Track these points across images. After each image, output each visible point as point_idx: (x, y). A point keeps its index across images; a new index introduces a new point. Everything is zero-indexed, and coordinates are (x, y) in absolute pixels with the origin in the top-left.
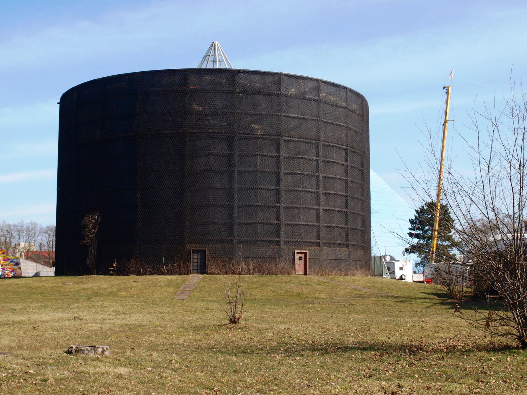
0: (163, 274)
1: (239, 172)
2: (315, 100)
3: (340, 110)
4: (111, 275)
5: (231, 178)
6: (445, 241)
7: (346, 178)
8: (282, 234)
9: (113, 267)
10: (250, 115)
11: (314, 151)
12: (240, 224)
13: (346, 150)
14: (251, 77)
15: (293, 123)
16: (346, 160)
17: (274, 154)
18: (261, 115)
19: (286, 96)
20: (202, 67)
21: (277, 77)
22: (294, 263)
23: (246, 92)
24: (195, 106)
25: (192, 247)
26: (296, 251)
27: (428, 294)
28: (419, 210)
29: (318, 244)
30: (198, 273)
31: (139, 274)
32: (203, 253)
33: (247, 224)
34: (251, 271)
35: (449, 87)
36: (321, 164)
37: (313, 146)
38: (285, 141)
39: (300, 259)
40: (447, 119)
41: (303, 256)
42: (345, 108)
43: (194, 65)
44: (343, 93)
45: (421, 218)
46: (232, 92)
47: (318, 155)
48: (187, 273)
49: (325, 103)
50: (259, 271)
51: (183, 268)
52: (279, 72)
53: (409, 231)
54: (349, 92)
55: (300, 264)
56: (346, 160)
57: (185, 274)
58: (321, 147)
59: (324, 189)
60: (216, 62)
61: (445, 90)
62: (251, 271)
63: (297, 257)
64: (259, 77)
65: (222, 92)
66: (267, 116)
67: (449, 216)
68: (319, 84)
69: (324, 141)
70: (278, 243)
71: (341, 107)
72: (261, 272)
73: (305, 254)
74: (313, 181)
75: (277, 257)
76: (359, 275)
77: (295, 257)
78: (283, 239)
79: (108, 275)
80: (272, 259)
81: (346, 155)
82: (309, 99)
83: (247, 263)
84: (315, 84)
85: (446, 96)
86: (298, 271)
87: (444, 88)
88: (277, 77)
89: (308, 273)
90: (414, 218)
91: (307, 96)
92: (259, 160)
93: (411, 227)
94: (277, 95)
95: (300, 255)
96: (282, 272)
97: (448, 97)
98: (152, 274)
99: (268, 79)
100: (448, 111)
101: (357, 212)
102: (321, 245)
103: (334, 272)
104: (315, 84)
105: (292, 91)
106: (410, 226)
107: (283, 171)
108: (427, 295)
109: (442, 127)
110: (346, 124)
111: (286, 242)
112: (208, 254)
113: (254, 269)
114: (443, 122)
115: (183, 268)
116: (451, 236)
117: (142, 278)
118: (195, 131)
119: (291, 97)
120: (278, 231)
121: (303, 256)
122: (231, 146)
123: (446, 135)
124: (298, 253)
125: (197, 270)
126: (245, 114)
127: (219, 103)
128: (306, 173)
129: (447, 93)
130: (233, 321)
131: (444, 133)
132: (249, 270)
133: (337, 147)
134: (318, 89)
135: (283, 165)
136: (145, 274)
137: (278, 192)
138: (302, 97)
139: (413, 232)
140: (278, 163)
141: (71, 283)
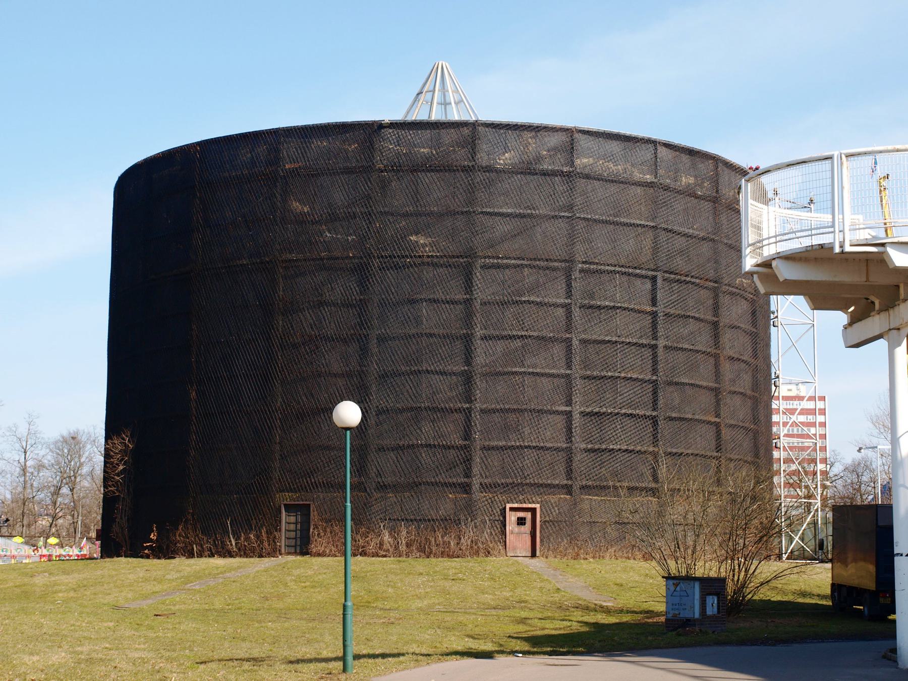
0: (230, 554)
1: (381, 340)
2: (561, 174)
4: (148, 557)
5: (364, 351)
8: (476, 470)
9: (151, 541)
10: (406, 215)
11: (561, 286)
12: (381, 449)
14: (410, 135)
15: (503, 227)
16: (654, 302)
17: (460, 297)
18: (430, 214)
19: (489, 169)
21: (466, 131)
22: (504, 533)
23: (396, 168)
24: (296, 206)
25: (287, 498)
26: (508, 506)
29: (568, 490)
30: (295, 553)
31: (191, 555)
32: (303, 510)
33: (398, 448)
34: (403, 548)
36: (576, 312)
37: (559, 274)
38: (484, 267)
39: (521, 522)
41: (528, 515)
42: (650, 185)
43: (397, 115)
46: (367, 169)
47: (569, 294)
48: (274, 552)
49: (587, 177)
50: (421, 550)
51: (266, 544)
54: (662, 151)
55: (519, 533)
57: (269, 555)
58: (576, 274)
59: (585, 367)
60: (450, 103)
62: (403, 548)
63: (512, 518)
64: (427, 134)
65: (348, 171)
66: (441, 215)
69: (583, 262)
70: (466, 488)
72: (426, 552)
73: (533, 511)
74: (558, 350)
75: (462, 517)
77: (505, 517)
78: (476, 482)
79: (142, 557)
80: (451, 523)
81: (654, 290)
82: (545, 174)
83: (394, 532)
86: (514, 549)
89: (538, 553)
91: (546, 166)
92: (425, 310)
94: (466, 170)
95: (521, 514)
96: (475, 551)
98: (212, 555)
99: (448, 137)
103: (611, 550)
105: (505, 159)
107: (479, 332)
111: (484, 487)
112: (314, 515)
113: (408, 545)
115: (266, 544)
117: (182, 566)
118: (294, 256)
120: (468, 461)
121: (528, 515)
122: (363, 284)
124: (512, 509)
125: (295, 546)
126: (392, 215)
127: (339, 194)
128: (535, 334)
132: (396, 548)
134: (275, 159)
135: (478, 319)
136: (200, 555)
137: (468, 379)
138: (528, 169)
140: (468, 318)
141: (129, 570)
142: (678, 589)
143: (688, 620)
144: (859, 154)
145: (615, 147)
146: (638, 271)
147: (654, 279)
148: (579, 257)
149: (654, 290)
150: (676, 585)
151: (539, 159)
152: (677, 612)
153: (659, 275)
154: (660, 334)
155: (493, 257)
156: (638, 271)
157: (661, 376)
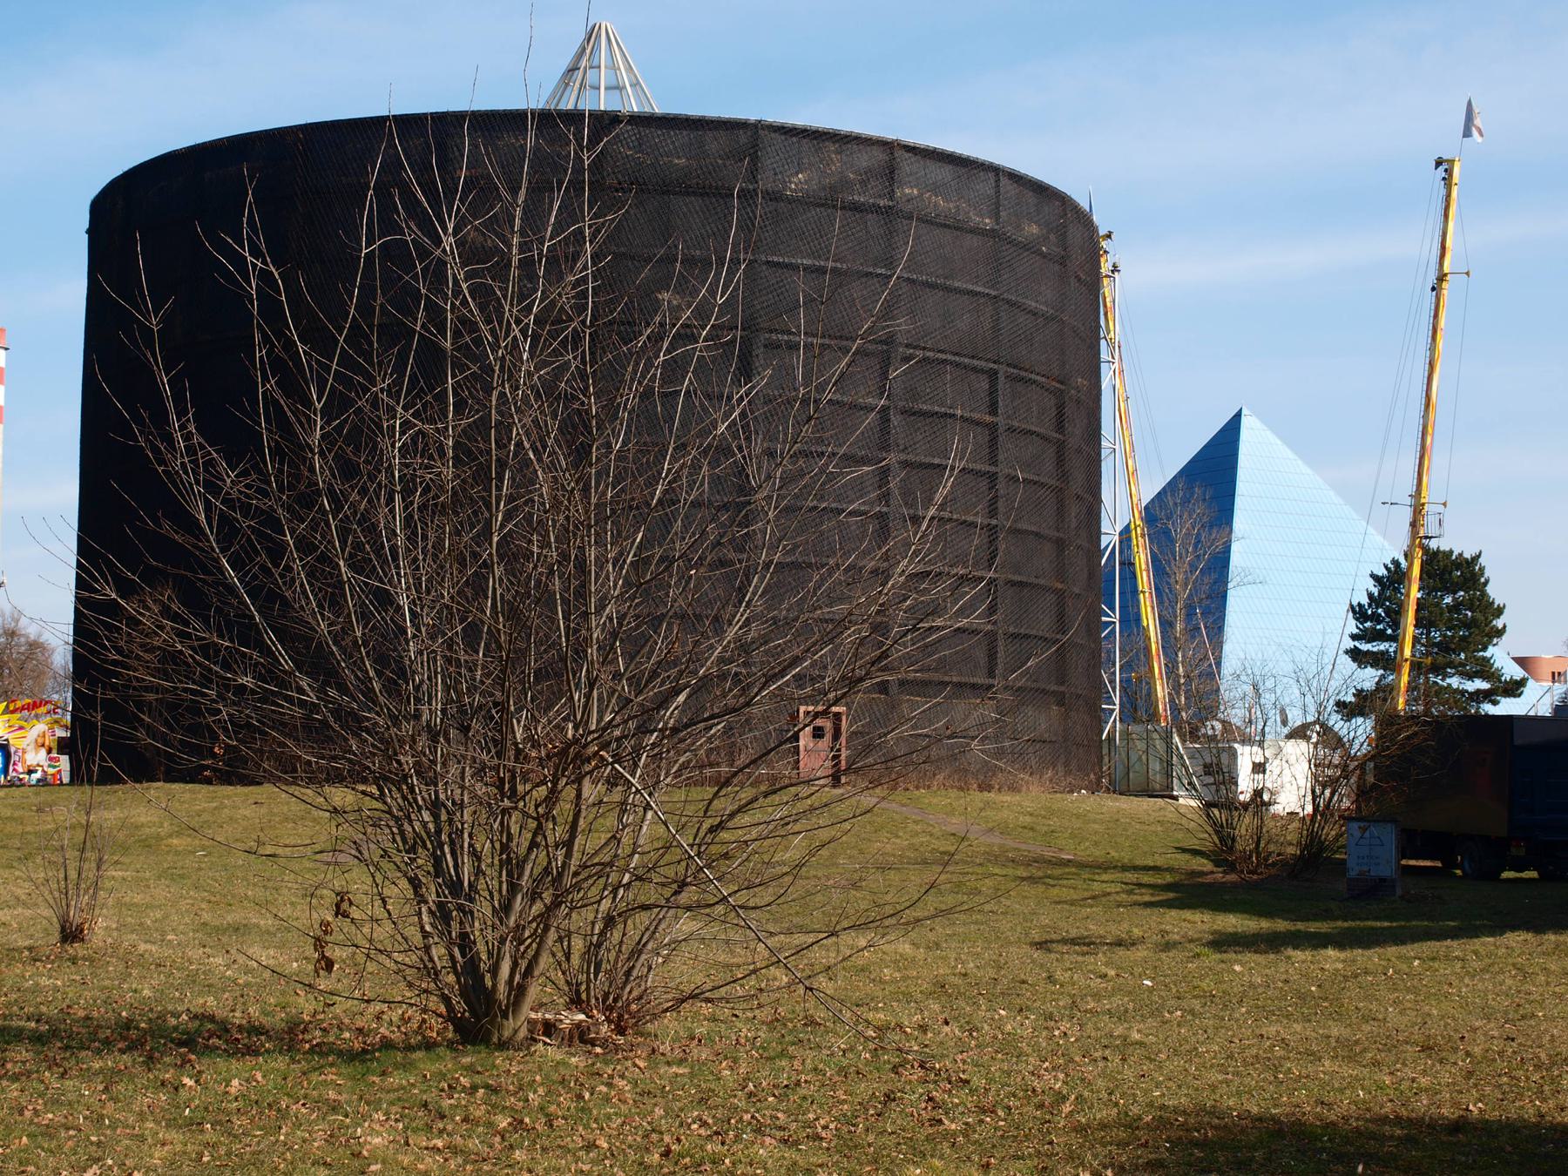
2: (876, 209)
3: (972, 241)
4: (208, 781)
6: (1470, 677)
7: (993, 469)
9: (214, 756)
13: (993, 375)
14: (656, 136)
19: (774, 197)
20: (562, 106)
21: (743, 137)
27: (1195, 852)
28: (1382, 572)
35: (1452, 162)
36: (895, 420)
40: (1446, 269)
42: (992, 233)
43: (534, 97)
44: (985, 186)
45: (1389, 599)
52: (753, 117)
53: (1350, 644)
54: (1004, 181)
56: (993, 411)
61: (1441, 172)
64: (683, 137)
67: (1484, 594)
68: (892, 155)
71: (975, 231)
76: (1035, 790)
81: (993, 392)
82: (856, 208)
84: (880, 155)
85: (1443, 192)
87: (1439, 163)
88: (743, 137)
90: (1365, 601)
93: (1356, 631)
97: (1448, 195)
100: (1449, 243)
101: (1032, 580)
102: (894, 689)
103: (940, 777)
104: (880, 155)
105: (798, 182)
106: (1352, 626)
108: (1187, 856)
109: (1430, 297)
110: (992, 287)
114: (1432, 279)
116: (1486, 661)
119: (790, 200)
123: (1442, 323)
126: (632, 258)
129: (1448, 180)
130: (71, 934)
131: (1436, 316)
133: (958, 365)
134: (890, 173)
138: (829, 200)
139: (1365, 647)
142: (1367, 834)
143: (1383, 880)
144: (1446, 216)
145: (944, 173)
146: (976, 362)
147: (993, 375)
148: (901, 339)
149: (993, 392)
150: (1364, 830)
151: (846, 184)
152: (1365, 868)
153: (1002, 369)
154: (1001, 457)
155: (783, 332)
156: (976, 362)
157: (1004, 521)
